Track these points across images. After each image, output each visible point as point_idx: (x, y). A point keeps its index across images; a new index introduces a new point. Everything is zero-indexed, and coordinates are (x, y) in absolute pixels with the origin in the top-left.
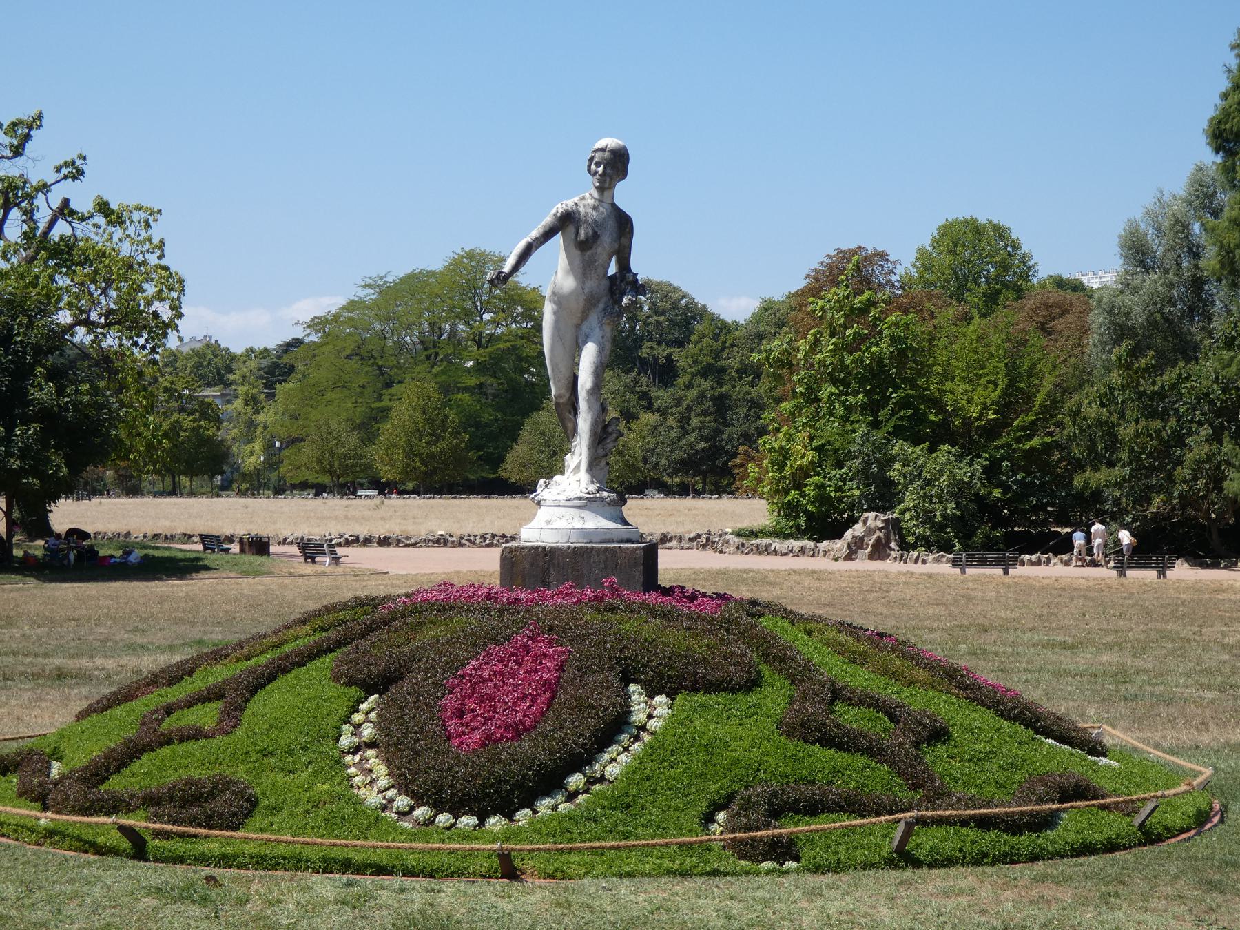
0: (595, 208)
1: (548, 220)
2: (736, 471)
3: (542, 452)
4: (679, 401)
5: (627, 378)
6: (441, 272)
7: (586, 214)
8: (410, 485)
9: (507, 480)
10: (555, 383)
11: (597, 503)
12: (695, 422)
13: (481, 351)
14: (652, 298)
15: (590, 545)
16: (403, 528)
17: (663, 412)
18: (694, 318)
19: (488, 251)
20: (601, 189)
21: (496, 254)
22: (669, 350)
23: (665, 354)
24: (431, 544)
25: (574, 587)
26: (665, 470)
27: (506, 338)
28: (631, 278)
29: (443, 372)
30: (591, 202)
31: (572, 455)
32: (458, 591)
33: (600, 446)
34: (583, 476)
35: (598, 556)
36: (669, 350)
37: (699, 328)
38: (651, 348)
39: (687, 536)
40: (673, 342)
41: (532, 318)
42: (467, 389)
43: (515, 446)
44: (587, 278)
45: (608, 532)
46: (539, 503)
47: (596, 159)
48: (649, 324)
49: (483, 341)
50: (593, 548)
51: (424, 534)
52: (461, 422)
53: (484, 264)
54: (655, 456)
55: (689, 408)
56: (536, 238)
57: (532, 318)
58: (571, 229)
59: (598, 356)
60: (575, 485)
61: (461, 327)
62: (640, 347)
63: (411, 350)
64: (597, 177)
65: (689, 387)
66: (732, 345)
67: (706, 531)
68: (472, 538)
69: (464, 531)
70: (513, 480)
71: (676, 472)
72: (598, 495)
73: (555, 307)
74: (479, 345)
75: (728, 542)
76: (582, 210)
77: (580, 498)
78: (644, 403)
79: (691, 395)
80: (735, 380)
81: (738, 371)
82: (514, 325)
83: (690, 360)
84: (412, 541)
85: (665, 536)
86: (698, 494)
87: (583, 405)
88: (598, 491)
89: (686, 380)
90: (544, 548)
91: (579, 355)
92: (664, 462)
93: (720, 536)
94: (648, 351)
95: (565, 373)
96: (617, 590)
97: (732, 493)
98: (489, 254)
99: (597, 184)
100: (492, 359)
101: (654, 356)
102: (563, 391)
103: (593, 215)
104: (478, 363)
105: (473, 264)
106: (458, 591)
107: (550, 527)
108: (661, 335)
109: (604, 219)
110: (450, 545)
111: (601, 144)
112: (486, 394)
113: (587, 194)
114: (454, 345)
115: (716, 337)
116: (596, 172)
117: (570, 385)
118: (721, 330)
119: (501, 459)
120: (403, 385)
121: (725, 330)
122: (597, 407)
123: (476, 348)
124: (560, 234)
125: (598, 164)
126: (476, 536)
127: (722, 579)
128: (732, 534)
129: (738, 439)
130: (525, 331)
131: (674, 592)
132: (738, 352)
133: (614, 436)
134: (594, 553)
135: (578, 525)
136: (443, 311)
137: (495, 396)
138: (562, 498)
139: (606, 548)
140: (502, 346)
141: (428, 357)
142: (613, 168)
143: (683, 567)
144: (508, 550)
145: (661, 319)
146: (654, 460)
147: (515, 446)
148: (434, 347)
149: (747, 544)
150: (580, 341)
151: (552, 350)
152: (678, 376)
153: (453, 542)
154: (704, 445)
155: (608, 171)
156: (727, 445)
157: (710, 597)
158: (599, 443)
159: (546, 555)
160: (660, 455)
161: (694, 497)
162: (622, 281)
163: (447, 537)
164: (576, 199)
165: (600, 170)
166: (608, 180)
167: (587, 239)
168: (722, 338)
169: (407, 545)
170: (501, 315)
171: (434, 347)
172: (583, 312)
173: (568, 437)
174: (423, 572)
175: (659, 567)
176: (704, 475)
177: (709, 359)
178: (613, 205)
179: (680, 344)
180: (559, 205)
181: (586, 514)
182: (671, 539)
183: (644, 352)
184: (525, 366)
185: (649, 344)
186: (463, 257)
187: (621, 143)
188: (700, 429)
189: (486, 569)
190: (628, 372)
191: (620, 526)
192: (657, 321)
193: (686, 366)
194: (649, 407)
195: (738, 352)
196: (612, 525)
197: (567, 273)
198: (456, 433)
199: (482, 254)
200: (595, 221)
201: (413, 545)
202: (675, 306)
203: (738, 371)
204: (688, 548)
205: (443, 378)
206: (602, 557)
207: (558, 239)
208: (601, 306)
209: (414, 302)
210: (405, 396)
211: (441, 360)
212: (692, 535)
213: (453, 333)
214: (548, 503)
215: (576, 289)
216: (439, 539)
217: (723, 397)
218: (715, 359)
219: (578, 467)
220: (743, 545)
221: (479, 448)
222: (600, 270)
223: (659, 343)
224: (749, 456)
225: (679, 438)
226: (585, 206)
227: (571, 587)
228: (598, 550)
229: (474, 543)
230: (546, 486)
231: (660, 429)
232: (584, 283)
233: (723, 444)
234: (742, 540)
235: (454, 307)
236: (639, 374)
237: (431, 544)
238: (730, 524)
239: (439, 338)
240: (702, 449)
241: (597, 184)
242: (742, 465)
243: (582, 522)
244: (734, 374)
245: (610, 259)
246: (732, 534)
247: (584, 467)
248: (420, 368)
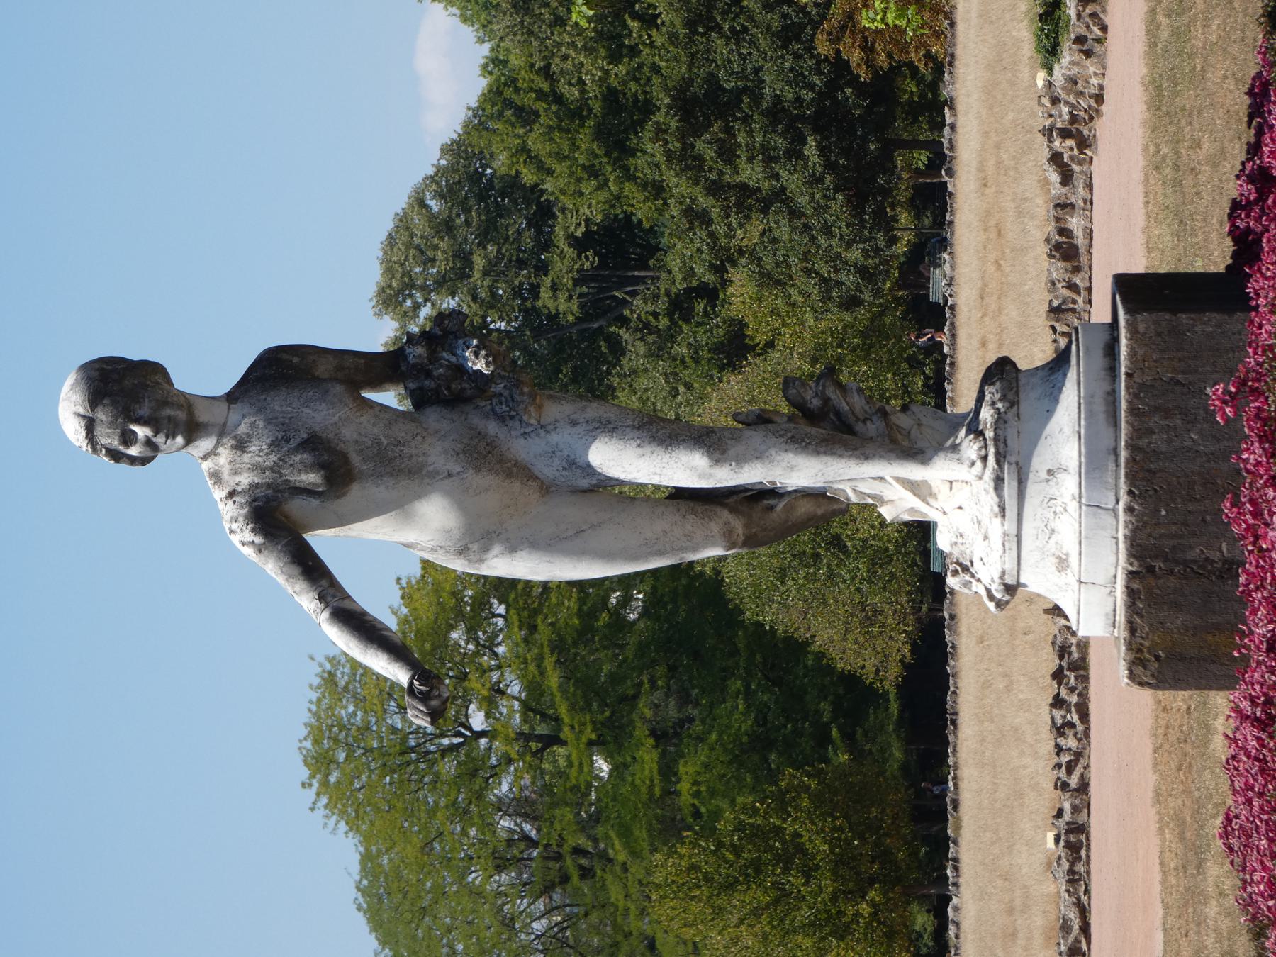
0: (240, 446)
1: (272, 568)
2: (882, 60)
3: (831, 574)
4: (697, 217)
5: (637, 351)
6: (367, 839)
7: (262, 469)
8: (922, 920)
9: (906, 666)
10: (695, 549)
11: (1011, 434)
12: (750, 173)
13: (566, 733)
14: (424, 288)
15: (1123, 454)
16: (1038, 940)
17: (723, 261)
18: (476, 177)
19: (306, 717)
20: (192, 431)
21: (314, 696)
22: (562, 243)
23: (570, 252)
24: (1081, 867)
25: (1236, 496)
26: (877, 250)
27: (532, 668)
28: (419, 351)
29: (626, 833)
30: (224, 457)
31: (882, 501)
32: (1249, 802)
33: (859, 427)
34: (938, 472)
35: (1150, 432)
36: (562, 243)
37: (501, 163)
38: (554, 288)
39: (1057, 189)
40: (539, 232)
41: (481, 603)
42: (668, 770)
43: (815, 647)
44: (422, 466)
45: (1086, 406)
46: (1011, 589)
47: (115, 443)
48: (494, 295)
49: (541, 729)
50: (1131, 447)
51: (1054, 886)
52: (753, 790)
53: (342, 727)
54: (842, 277)
55: (715, 189)
56: (321, 598)
57: (481, 603)
58: (297, 507)
59: (622, 437)
60: (962, 495)
61: (505, 787)
62: (553, 317)
63: (569, 917)
64: (160, 439)
65: (658, 190)
66: (546, 72)
67: (1041, 140)
68: (1065, 758)
69: (1047, 781)
70: (906, 651)
71: (885, 223)
72: (989, 434)
73: (496, 549)
74: (553, 740)
75: (1073, 81)
76: (245, 480)
77: (999, 481)
78: (700, 306)
79: (679, 185)
80: (641, 66)
81: (614, 58)
82: (501, 650)
83: (588, 187)
84: (1073, 915)
85: (1057, 247)
86: (940, 160)
87: (751, 475)
88: (980, 434)
89: (640, 196)
90: (1132, 575)
91: (622, 483)
92: (855, 255)
93: (1055, 101)
94: (562, 296)
95: (669, 522)
96: (1244, 383)
97: (939, 70)
98: (317, 715)
99: (180, 440)
100: (587, 707)
101: (576, 282)
102: (715, 527)
103: (258, 452)
104: (598, 744)
105: (342, 756)
106: (1249, 802)
107: (1074, 560)
108: (521, 264)
109: (268, 422)
110: (1082, 818)
111: (74, 431)
112: (681, 723)
113: (206, 466)
114: (554, 805)
115: (526, 117)
116: (149, 443)
117: (700, 508)
118: (509, 103)
119: (851, 680)
120: (660, 936)
121: (509, 93)
122: (755, 437)
123: (560, 750)
124: (304, 535)
125: (128, 439)
126: (1059, 750)
127: (1175, 94)
128: (1050, 70)
129: (797, 56)
130: (515, 618)
131: (1248, 230)
132: (565, 58)
133: (831, 392)
134: (1143, 443)
135: (1068, 485)
136: (464, 833)
137: (684, 700)
138: (996, 528)
139: (1132, 410)
140: (553, 680)
141: (586, 873)
142: (138, 400)
143: (1141, 199)
144: (1139, 670)
145: (479, 262)
146: (850, 279)
147: (815, 647)
148: (559, 857)
149: (1077, 29)
150: (584, 483)
151: (608, 556)
152: (628, 216)
153: (1075, 809)
154: (811, 149)
155: (145, 411)
156: (811, 87)
157: (1260, 133)
158: (850, 431)
159: (1151, 570)
160: (836, 261)
161: (950, 173)
162: (428, 374)
163: (1061, 823)
164: (219, 494)
165: (141, 432)
166: (168, 412)
167: (321, 466)
168: (528, 100)
169: (1085, 929)
170: (474, 683)
171: (559, 857)
172: (509, 475)
173: (835, 513)
174: (1157, 888)
175: (1140, 269)
176: (891, 146)
177: (585, 139)
178: (232, 397)
179: (543, 214)
180: (235, 539)
181: (1039, 464)
182: (1063, 232)
183: (566, 306)
184: (605, 616)
185: (545, 294)
186: (325, 783)
187: (71, 379)
188: (769, 160)
189: (1150, 722)
190: (618, 349)
191: (1072, 375)
192: (485, 273)
193: (603, 195)
194: (710, 294)
195: (565, 58)
196: (1070, 397)
197: (408, 518)
198: (782, 804)
199: (316, 734)
200: (275, 444)
201: (1084, 912)
202: (445, 226)
203: (614, 58)
204: (1090, 186)
205: (641, 833)
206: (1156, 420)
207: (321, 540)
208: (492, 428)
209: (443, 912)
210: (688, 933)
211: (595, 841)
212: (1054, 177)
213: (520, 807)
214: (1010, 565)
215: (448, 493)
216: (1068, 845)
217: (685, 104)
218: (583, 119)
219: (918, 488)
220: (1080, 40)
221: (823, 739)
222: (401, 431)
223: (543, 268)
224: (843, 28)
225: (795, 213)
226: (235, 472)
227: (1236, 503)
228: (1138, 432)
229: (1078, 755)
230: (966, 569)
231: (769, 265)
232: (433, 475)
233: (807, 95)
234: (1066, 47)
235: (455, 803)
236: (624, 321)
237: (1081, 867)
238: (1025, 72)
239: (533, 843)
240: (823, 151)
241: (180, 440)
242: (868, 48)
243: (1061, 476)
244: (622, 69)
245: (370, 404)
246: (1050, 70)
247: (913, 471)
248: (615, 893)
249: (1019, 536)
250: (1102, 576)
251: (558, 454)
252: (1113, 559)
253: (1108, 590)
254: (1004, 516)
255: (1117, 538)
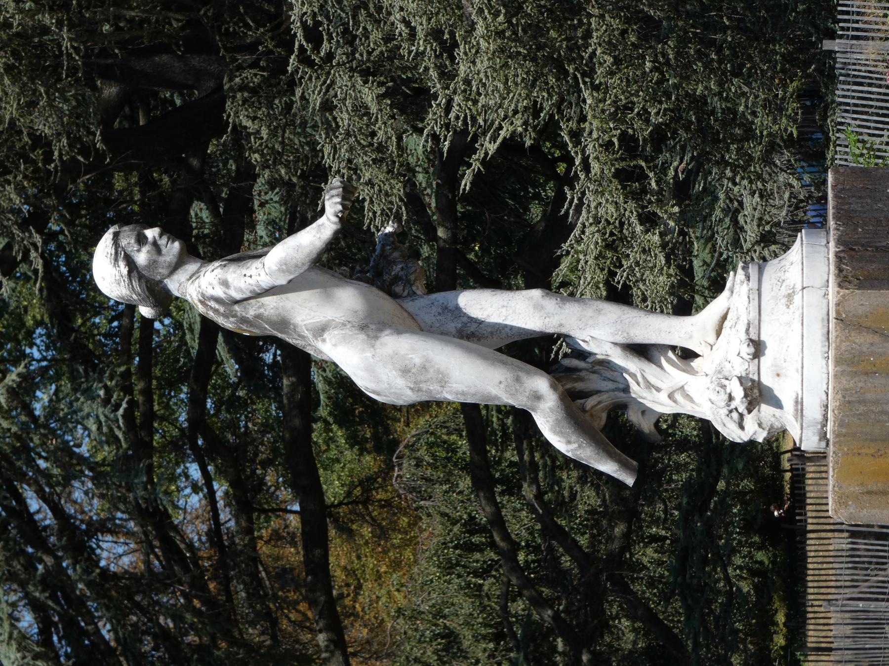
249: (759, 290)
250: (819, 281)
251: (436, 303)
252: (826, 269)
253: (822, 292)
254: (749, 280)
255: (828, 259)
